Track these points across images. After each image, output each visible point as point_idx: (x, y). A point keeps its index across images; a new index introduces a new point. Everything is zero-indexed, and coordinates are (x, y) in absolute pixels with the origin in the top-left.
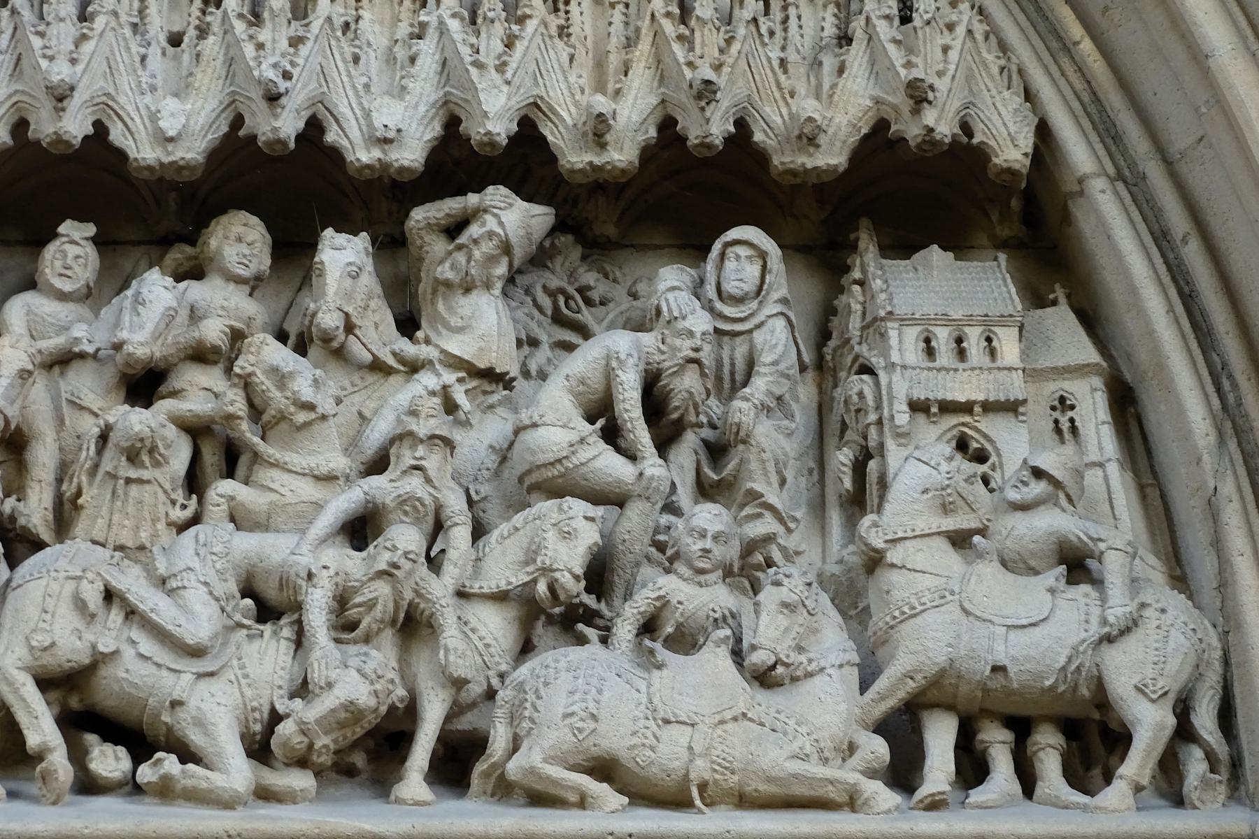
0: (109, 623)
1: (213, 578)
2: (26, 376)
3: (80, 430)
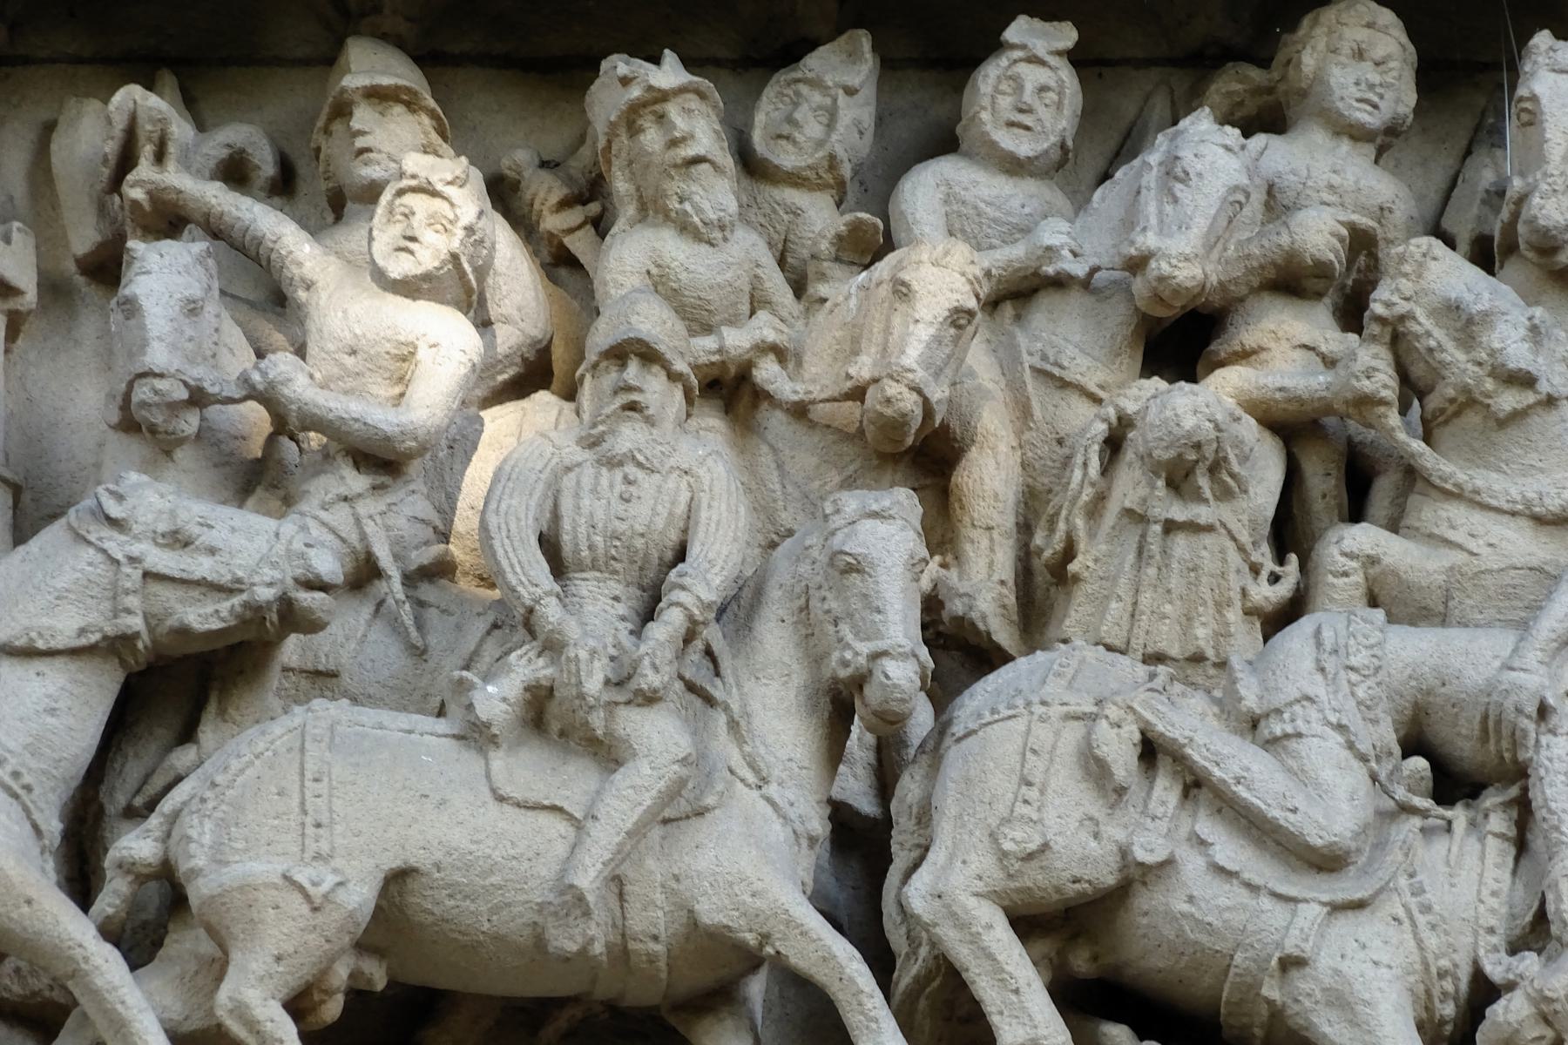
0: (1152, 805)
1: (1352, 718)
2: (962, 322)
3: (1064, 429)
